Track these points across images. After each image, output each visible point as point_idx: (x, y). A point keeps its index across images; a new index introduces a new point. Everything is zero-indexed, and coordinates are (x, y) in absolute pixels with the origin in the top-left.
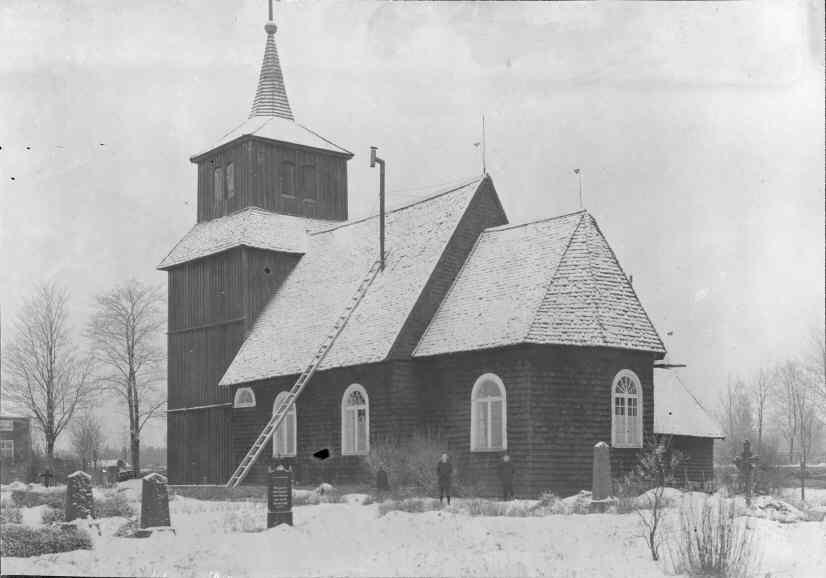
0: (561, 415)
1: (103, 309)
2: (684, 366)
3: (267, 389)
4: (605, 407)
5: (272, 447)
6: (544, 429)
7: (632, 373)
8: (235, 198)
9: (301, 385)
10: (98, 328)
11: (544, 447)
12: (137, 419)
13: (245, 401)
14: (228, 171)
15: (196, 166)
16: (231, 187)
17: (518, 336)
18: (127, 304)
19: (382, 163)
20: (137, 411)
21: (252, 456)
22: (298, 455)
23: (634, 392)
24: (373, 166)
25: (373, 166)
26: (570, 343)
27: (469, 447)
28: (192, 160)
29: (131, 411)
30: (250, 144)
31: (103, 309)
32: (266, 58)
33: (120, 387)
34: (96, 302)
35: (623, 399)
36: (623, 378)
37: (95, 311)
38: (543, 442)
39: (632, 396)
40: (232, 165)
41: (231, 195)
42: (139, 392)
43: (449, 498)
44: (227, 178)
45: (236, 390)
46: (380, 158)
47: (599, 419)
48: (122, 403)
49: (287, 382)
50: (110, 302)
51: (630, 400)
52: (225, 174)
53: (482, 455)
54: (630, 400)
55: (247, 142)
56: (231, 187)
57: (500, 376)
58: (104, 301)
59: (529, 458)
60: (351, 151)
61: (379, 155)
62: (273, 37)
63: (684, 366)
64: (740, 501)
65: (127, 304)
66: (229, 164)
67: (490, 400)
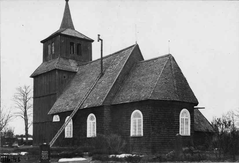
2: (204, 108)
4: (178, 122)
5: (65, 133)
7: (94, 115)
8: (55, 53)
9: (73, 114)
12: (27, 125)
13: (56, 119)
14: (53, 45)
16: (53, 50)
19: (102, 40)
20: (27, 123)
21: (56, 137)
22: (73, 137)
23: (187, 117)
24: (98, 41)
25: (98, 41)
27: (130, 135)
28: (42, 42)
35: (183, 119)
36: (184, 112)
39: (187, 118)
40: (54, 43)
44: (52, 49)
45: (53, 116)
47: (175, 126)
49: (69, 113)
51: (186, 119)
52: (52, 46)
53: (134, 137)
54: (186, 119)
56: (53, 50)
59: (151, 139)
60: (94, 40)
61: (100, 38)
63: (204, 108)
64: (194, 117)
67: (137, 119)
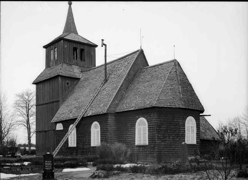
0: (168, 132)
1: (18, 98)
2: (210, 115)
3: (67, 123)
6: (161, 137)
9: (77, 122)
10: (17, 104)
11: (161, 144)
13: (60, 127)
15: (45, 49)
17: (154, 103)
18: (27, 97)
19: (105, 45)
22: (77, 146)
24: (102, 46)
26: (171, 107)
29: (28, 131)
30: (62, 41)
31: (18, 98)
32: (68, 18)
33: (25, 124)
34: (15, 96)
37: (16, 99)
38: (161, 142)
40: (56, 48)
41: (56, 59)
42: (30, 125)
43: (74, 81)
46: (105, 43)
47: (181, 134)
48: (26, 129)
49: (72, 121)
50: (22, 96)
53: (139, 146)
54: (192, 127)
55: (61, 40)
56: (56, 56)
57: (145, 118)
58: (19, 96)
59: (156, 148)
61: (104, 42)
62: (71, 6)
63: (210, 115)
65: (27, 97)
66: (55, 48)
67: (142, 127)
